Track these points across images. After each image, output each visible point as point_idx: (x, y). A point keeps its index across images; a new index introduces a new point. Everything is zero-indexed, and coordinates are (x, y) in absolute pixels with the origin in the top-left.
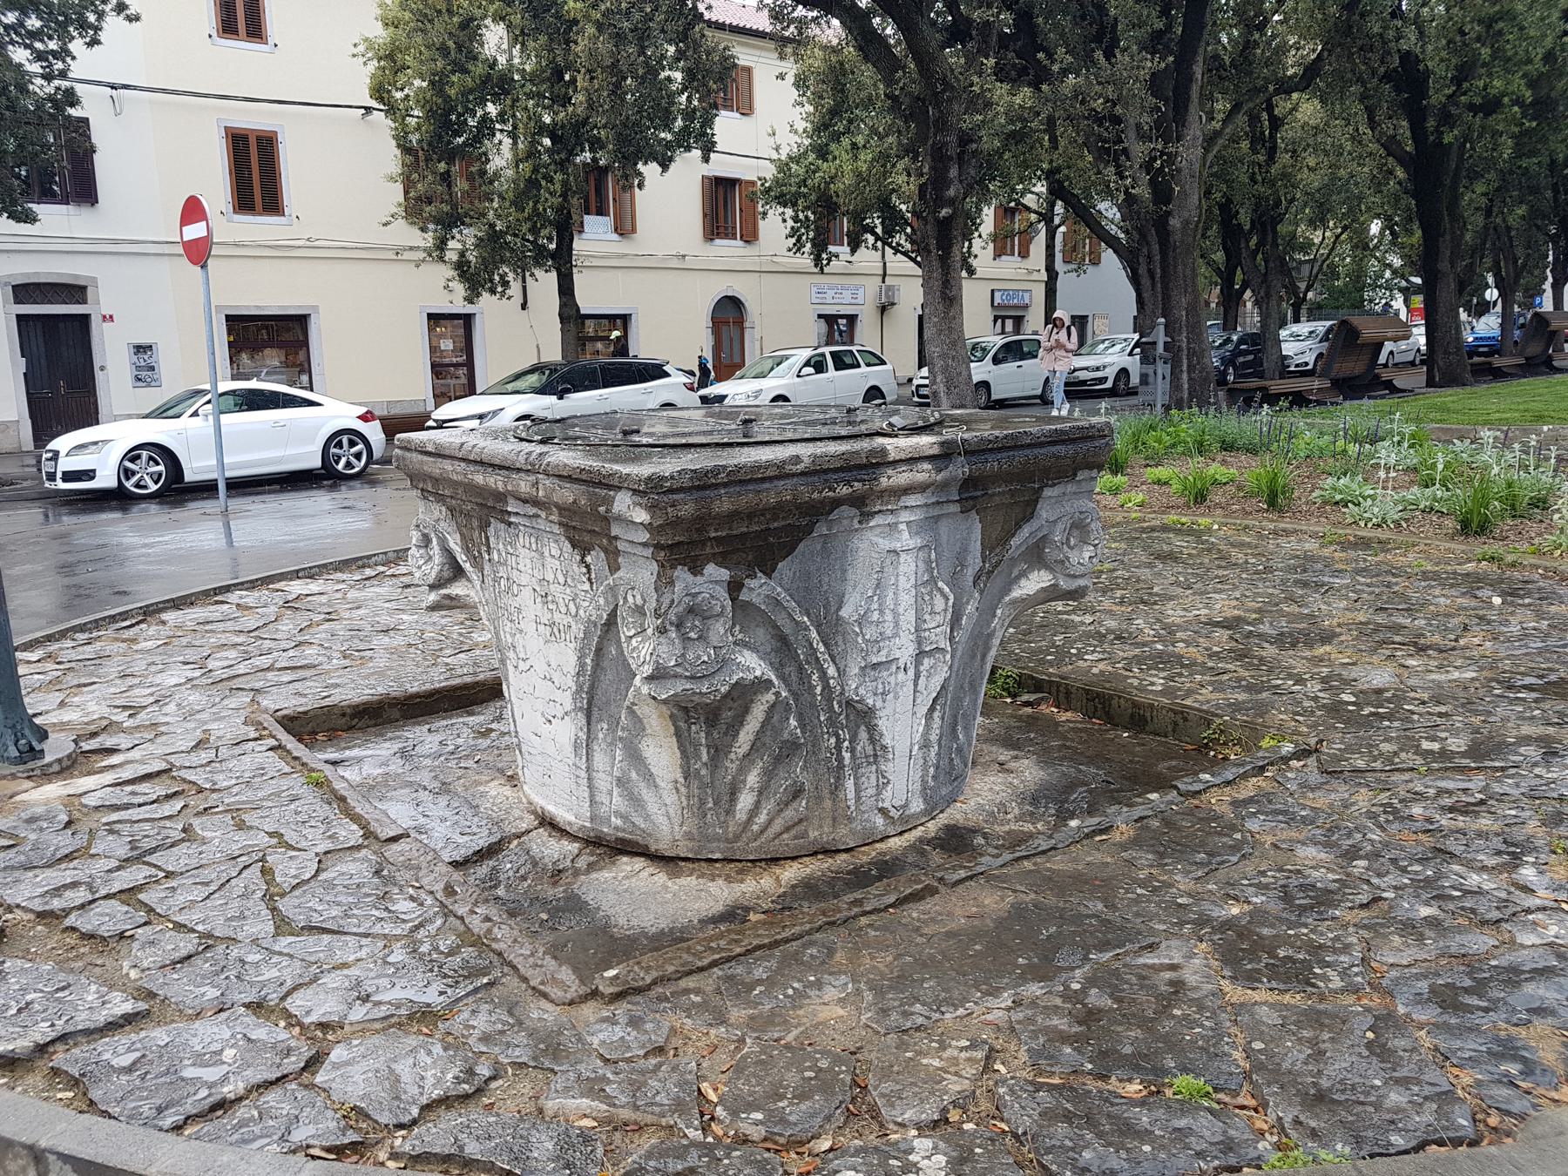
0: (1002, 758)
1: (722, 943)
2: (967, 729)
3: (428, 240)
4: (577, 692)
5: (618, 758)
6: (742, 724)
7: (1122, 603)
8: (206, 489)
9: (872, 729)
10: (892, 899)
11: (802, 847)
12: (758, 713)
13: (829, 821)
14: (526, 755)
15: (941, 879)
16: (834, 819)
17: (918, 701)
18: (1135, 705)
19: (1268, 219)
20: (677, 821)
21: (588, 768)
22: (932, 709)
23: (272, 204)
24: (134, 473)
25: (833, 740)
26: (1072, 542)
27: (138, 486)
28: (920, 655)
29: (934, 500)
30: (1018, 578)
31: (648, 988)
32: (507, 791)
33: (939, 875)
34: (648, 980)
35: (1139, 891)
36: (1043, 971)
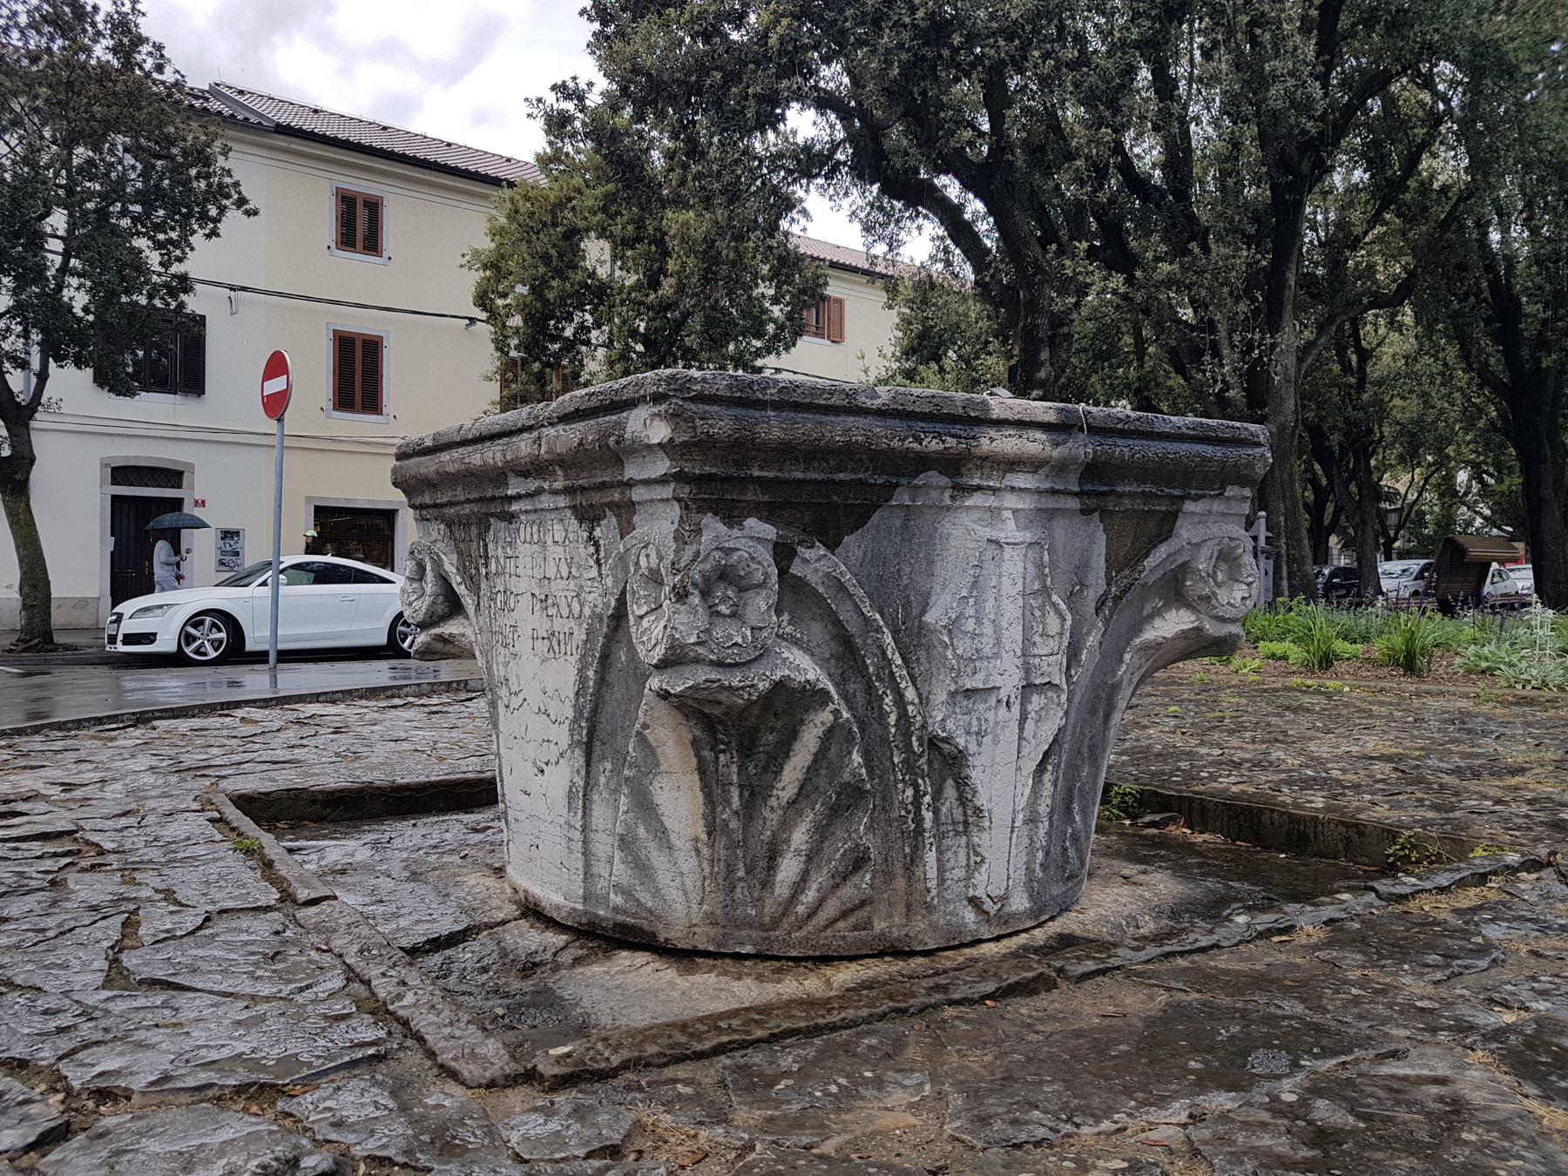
0: (1126, 872)
1: (735, 1023)
2: (1084, 812)
4: (576, 720)
5: (623, 808)
6: (787, 756)
7: (1253, 742)
8: (260, 657)
9: (962, 782)
10: (990, 987)
11: (864, 943)
13: (901, 909)
15: (1060, 971)
16: (909, 907)
17: (1025, 752)
18: (1293, 819)
19: (1361, 443)
20: (695, 896)
21: (584, 828)
22: (1041, 768)
23: (372, 404)
24: (195, 639)
25: (910, 792)
26: (1220, 576)
27: (197, 652)
28: (1028, 688)
29: (1046, 485)
30: (1151, 617)
31: (614, 1073)
32: (491, 882)
33: (1058, 964)
34: (615, 1060)
35: (1354, 991)
36: (1231, 1075)
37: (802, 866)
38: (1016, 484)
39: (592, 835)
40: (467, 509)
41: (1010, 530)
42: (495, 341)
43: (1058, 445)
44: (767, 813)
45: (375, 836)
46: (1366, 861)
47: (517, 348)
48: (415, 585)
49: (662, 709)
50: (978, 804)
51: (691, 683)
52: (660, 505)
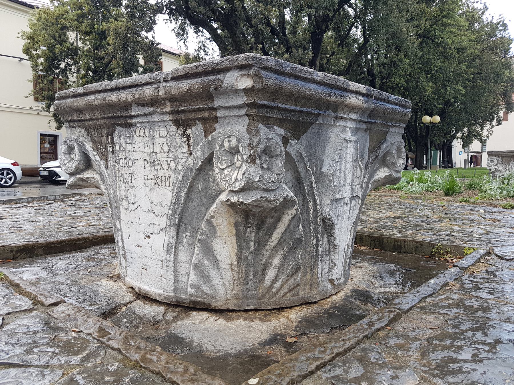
3: (43, 104)
4: (173, 215)
12: (286, 220)
14: (130, 260)
16: (311, 285)
20: (230, 288)
21: (174, 261)
25: (315, 240)
28: (352, 197)
29: (359, 118)
37: (276, 273)
38: (352, 117)
39: (178, 264)
40: (102, 122)
41: (349, 136)
42: (33, 67)
43: (366, 102)
44: (264, 252)
45: (46, 265)
46: (423, 254)
47: (42, 70)
48: (67, 156)
49: (223, 211)
50: (336, 243)
51: (255, 199)
52: (236, 119)
